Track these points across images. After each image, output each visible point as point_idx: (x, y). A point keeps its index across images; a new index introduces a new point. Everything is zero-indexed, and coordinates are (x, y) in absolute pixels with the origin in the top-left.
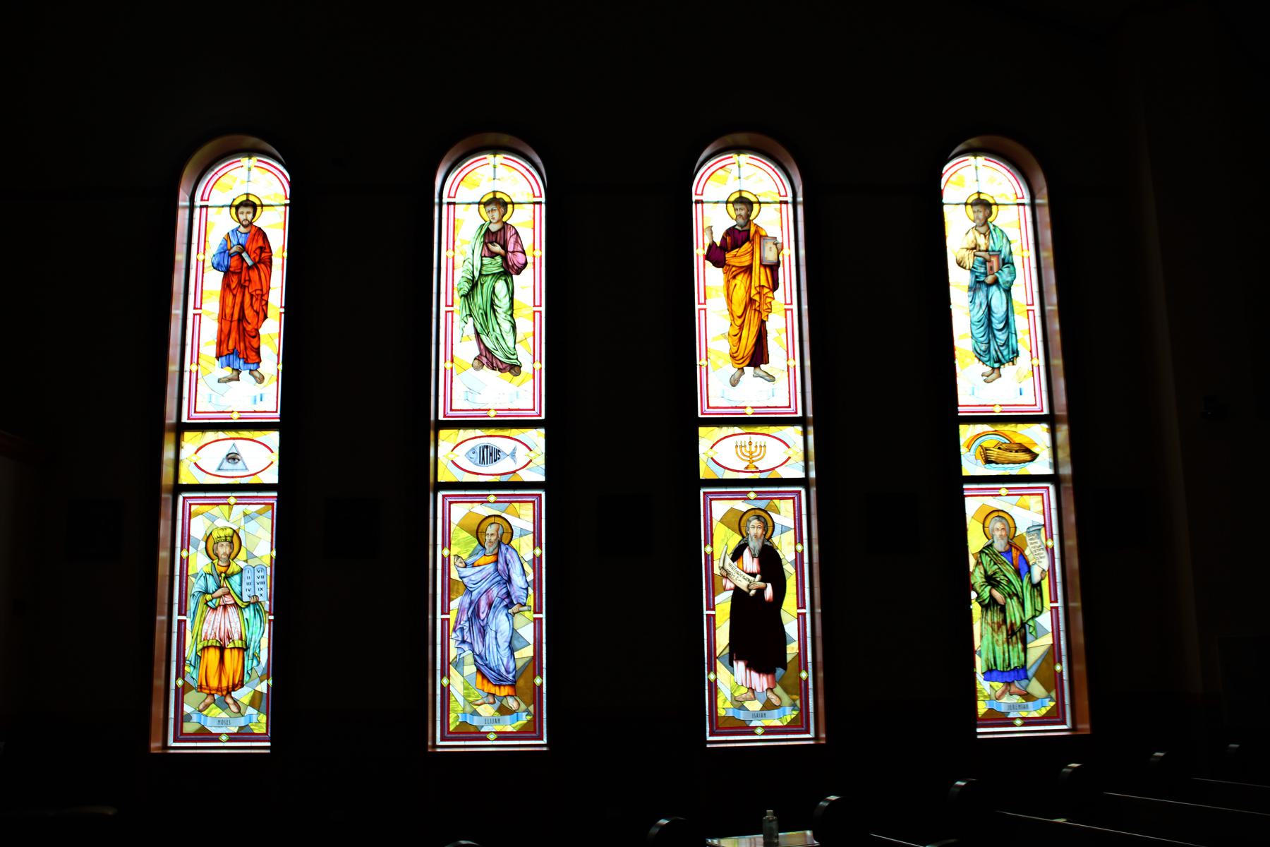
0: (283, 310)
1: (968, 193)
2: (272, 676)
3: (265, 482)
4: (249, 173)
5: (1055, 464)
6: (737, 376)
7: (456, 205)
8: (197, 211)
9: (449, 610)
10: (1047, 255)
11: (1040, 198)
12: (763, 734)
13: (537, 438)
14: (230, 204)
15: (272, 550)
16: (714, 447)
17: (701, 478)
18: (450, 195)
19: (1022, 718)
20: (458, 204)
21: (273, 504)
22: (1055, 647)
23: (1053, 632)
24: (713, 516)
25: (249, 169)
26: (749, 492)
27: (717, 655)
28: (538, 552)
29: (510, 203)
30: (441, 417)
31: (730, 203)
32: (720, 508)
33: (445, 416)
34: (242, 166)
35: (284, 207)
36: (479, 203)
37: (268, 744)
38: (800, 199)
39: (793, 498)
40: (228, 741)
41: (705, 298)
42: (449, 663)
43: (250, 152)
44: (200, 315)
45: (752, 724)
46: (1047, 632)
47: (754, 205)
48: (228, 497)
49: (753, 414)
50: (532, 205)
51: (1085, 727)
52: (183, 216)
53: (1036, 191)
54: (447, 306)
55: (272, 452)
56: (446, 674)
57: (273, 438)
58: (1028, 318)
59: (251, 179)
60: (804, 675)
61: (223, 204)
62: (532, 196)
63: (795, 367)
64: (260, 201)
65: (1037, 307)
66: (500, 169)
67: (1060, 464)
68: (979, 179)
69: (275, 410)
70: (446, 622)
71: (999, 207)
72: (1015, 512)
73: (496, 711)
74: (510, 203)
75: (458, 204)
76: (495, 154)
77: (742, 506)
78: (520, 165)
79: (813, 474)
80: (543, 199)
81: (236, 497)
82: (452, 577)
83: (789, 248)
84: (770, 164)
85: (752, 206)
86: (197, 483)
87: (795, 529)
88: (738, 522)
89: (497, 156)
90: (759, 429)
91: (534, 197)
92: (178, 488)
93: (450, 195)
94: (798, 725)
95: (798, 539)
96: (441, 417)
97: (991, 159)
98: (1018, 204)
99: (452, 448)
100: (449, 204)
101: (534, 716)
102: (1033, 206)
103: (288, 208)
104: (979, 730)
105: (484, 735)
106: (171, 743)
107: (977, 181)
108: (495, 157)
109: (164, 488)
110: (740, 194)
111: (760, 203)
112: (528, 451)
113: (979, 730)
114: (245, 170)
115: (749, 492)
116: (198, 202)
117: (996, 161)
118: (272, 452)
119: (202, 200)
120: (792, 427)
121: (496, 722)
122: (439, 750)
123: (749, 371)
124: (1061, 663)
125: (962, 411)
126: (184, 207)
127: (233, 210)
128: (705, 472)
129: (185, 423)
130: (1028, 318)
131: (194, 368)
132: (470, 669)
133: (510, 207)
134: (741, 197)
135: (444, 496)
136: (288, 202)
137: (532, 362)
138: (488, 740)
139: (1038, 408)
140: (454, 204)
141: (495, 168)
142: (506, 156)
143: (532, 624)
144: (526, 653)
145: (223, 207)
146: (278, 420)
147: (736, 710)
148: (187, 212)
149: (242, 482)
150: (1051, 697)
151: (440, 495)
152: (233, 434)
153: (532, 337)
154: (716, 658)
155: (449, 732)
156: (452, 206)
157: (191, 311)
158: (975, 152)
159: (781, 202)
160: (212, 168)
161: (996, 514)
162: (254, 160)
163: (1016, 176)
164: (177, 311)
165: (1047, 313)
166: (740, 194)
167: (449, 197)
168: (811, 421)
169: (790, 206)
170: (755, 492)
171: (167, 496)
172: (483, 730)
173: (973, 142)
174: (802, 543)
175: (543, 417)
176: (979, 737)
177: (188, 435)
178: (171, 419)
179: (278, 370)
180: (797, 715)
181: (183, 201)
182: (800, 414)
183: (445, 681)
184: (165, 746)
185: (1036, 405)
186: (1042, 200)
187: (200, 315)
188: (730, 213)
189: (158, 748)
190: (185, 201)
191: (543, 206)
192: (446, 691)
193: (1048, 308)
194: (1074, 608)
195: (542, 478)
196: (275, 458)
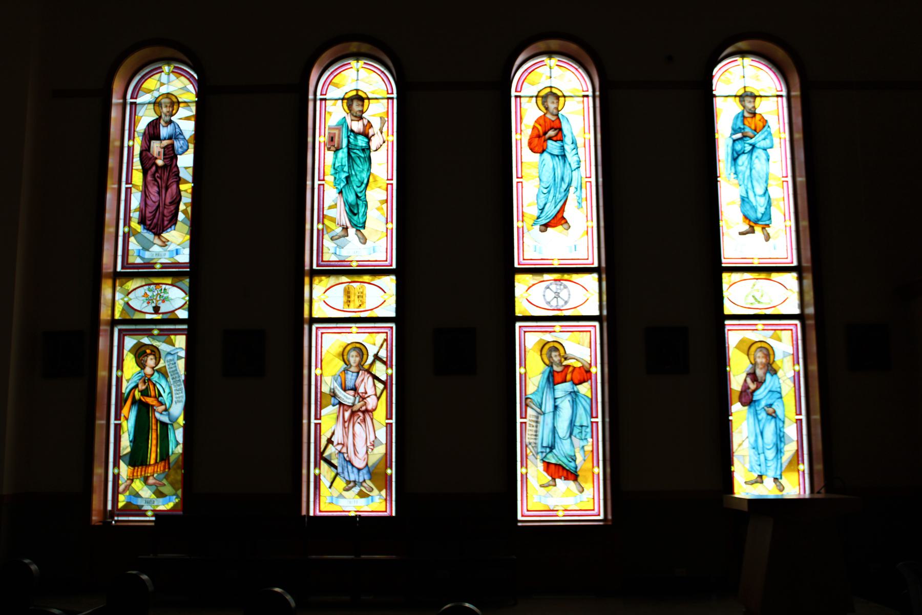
0: (719, 179)
5: (802, 305)
8: (318, 103)
9: (320, 416)
10: (798, 136)
11: (794, 91)
13: (389, 283)
18: (322, 93)
22: (387, 455)
23: (386, 444)
26: (153, 329)
28: (797, 368)
36: (343, 99)
37: (311, 514)
38: (597, 93)
41: (324, 176)
44: (323, 185)
45: (144, 508)
46: (381, 444)
49: (358, 266)
52: (115, 113)
53: (791, 86)
54: (517, 178)
58: (783, 188)
59: (359, 78)
60: (389, 471)
62: (386, 92)
64: (366, 95)
65: (790, 179)
72: (773, 343)
73: (154, 493)
78: (178, 73)
79: (605, 312)
80: (395, 95)
82: (323, 391)
83: (589, 132)
88: (748, 347)
89: (360, 61)
91: (388, 93)
92: (313, 321)
93: (322, 93)
96: (315, 267)
97: (570, 63)
98: (778, 96)
99: (324, 291)
100: (321, 100)
108: (743, 59)
109: (101, 321)
110: (357, 92)
112: (383, 293)
117: (757, 60)
119: (516, 91)
120: (388, 277)
125: (725, 262)
129: (120, 272)
130: (783, 188)
134: (357, 95)
135: (317, 328)
138: (146, 516)
139: (590, 261)
140: (325, 100)
141: (358, 71)
142: (560, 59)
143: (385, 428)
144: (381, 450)
147: (132, 497)
150: (381, 495)
151: (314, 327)
158: (743, 53)
159: (584, 96)
162: (361, 63)
163: (777, 74)
166: (357, 92)
167: (321, 95)
169: (591, 99)
173: (742, 45)
175: (394, 266)
181: (116, 100)
185: (386, 261)
186: (796, 93)
187: (323, 185)
188: (157, 112)
191: (395, 101)
195: (393, 314)
196: (726, 293)
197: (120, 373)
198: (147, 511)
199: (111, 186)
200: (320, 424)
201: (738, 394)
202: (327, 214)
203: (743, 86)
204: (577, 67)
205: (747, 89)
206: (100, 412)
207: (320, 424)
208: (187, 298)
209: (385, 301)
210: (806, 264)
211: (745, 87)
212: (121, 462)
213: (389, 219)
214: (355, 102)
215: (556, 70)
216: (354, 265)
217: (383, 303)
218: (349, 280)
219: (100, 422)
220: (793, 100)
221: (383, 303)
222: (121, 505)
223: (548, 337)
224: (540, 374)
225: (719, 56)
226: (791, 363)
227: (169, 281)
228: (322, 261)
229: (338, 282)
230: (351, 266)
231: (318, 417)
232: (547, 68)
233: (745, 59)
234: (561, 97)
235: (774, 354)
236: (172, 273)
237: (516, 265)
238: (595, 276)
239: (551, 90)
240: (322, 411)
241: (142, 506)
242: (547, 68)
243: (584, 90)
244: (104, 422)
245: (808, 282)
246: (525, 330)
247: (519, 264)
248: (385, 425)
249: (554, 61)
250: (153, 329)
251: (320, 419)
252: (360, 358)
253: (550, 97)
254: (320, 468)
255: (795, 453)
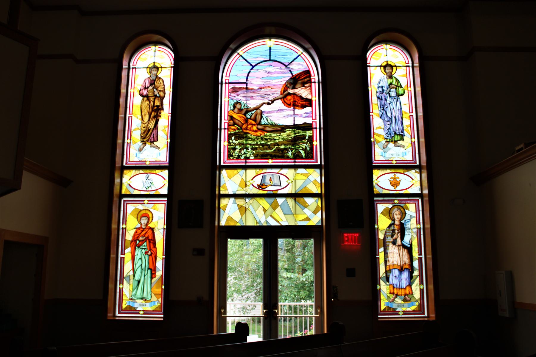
0: (170, 115)
1: (382, 61)
2: (164, 284)
3: (161, 194)
4: (386, 51)
5: (422, 189)
7: (136, 69)
8: (131, 70)
12: (403, 315)
15: (164, 225)
16: (131, 179)
20: (137, 68)
21: (165, 204)
24: (127, 211)
26: (395, 200)
27: (125, 275)
29: (160, 68)
30: (222, 164)
31: (382, 66)
32: (381, 208)
35: (170, 68)
36: (381, 66)
37: (162, 316)
39: (415, 203)
40: (403, 315)
42: (123, 278)
43: (156, 43)
45: (397, 310)
47: (159, 69)
49: (149, 164)
50: (405, 67)
55: (165, 179)
56: (122, 282)
61: (377, 65)
63: (224, 142)
66: (389, 50)
68: (387, 55)
69: (166, 160)
70: (123, 259)
71: (397, 67)
75: (137, 68)
76: (155, 46)
82: (126, 239)
84: (400, 48)
85: (158, 69)
87: (416, 217)
90: (154, 172)
91: (406, 63)
92: (122, 196)
96: (222, 164)
97: (142, 50)
99: (129, 178)
102: (413, 67)
103: (172, 69)
105: (397, 313)
106: (117, 314)
107: (387, 55)
108: (155, 47)
111: (162, 67)
115: (395, 200)
116: (132, 66)
118: (165, 179)
122: (117, 318)
123: (148, 145)
127: (382, 68)
128: (377, 190)
131: (413, 140)
136: (173, 65)
141: (155, 51)
145: (377, 66)
146: (168, 165)
148: (127, 70)
152: (148, 171)
154: (123, 278)
157: (414, 114)
162: (157, 47)
167: (133, 65)
169: (411, 68)
170: (398, 200)
171: (116, 199)
172: (138, 309)
178: (118, 165)
179: (167, 142)
181: (125, 66)
183: (121, 286)
190: (126, 65)
192: (121, 290)
194: (113, 254)
196: (166, 182)
199: (421, 114)
201: (129, 243)
202: (376, 132)
203: (153, 62)
204: (402, 50)
205: (156, 64)
206: (113, 250)
209: (165, 184)
210: (424, 163)
211: (154, 63)
212: (381, 281)
213: (413, 136)
214: (388, 67)
216: (148, 164)
217: (164, 186)
218: (144, 172)
219: (429, 256)
220: (415, 69)
221: (164, 186)
222: (124, 306)
223: (140, 207)
224: (135, 228)
227: (401, 171)
228: (413, 160)
229: (386, 172)
230: (268, 163)
231: (123, 253)
232: (384, 50)
233: (387, 45)
234: (160, 68)
236: (405, 167)
238: (318, 171)
240: (125, 250)
241: (137, 308)
242: (384, 50)
243: (407, 63)
244: (428, 256)
245: (424, 175)
246: (417, 204)
247: (224, 163)
248: (162, 259)
249: (388, 46)
251: (124, 254)
253: (388, 67)
254: (123, 285)
255: (160, 277)
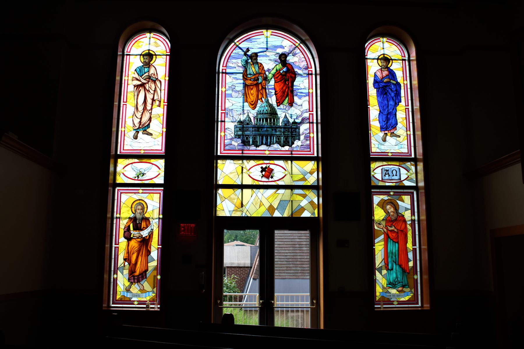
6: (136, 134)
9: (118, 243)
14: (140, 54)
17: (163, 183)
19: (397, 301)
25: (150, 38)
26: (390, 192)
30: (219, 154)
31: (142, 55)
33: (221, 153)
34: (146, 37)
36: (141, 55)
45: (132, 299)
46: (154, 260)
48: (139, 190)
51: (427, 306)
55: (160, 169)
57: (161, 163)
64: (155, 53)
67: (419, 181)
74: (154, 55)
77: (385, 197)
81: (142, 190)
86: (124, 182)
89: (151, 34)
91: (402, 57)
94: (152, 301)
95: (413, 214)
101: (414, 294)
104: (376, 306)
113: (376, 306)
114: (148, 39)
121: (394, 295)
124: (417, 275)
126: (120, 55)
129: (119, 154)
132: (126, 272)
133: (154, 57)
137: (162, 127)
138: (134, 304)
140: (129, 55)
149: (145, 183)
153: (162, 116)
155: (116, 300)
156: (129, 56)
160: (132, 37)
161: (138, 202)
164: (116, 103)
165: (414, 110)
168: (321, 159)
174: (414, 216)
176: (376, 310)
177: (120, 161)
178: (113, 153)
180: (413, 295)
182: (316, 155)
184: (109, 306)
189: (105, 307)
190: (120, 52)
193: (415, 107)
197: (413, 218)
198: (394, 301)
200: (118, 247)
207: (118, 247)
208: (372, 173)
215: (386, 45)
218: (139, 161)
225: (367, 38)
226: (410, 215)
232: (381, 43)
235: (147, 208)
237: (219, 154)
239: (384, 55)
244: (422, 247)
248: (412, 249)
250: (390, 192)
251: (118, 244)
252: (393, 208)
253: (386, 60)
